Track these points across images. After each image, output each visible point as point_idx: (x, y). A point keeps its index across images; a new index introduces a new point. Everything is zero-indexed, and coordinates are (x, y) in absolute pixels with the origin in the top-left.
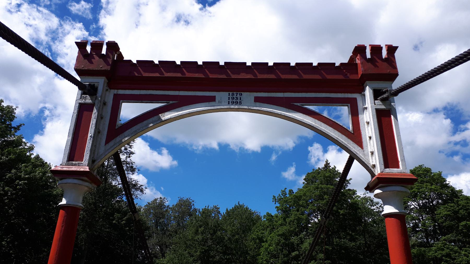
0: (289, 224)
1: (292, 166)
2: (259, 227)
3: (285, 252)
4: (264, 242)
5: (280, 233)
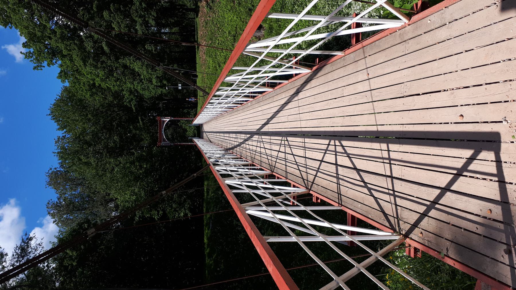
0: (70, 50)
1: (5, 49)
2: (76, 89)
3: (104, 58)
4: (94, 84)
5: (82, 63)
